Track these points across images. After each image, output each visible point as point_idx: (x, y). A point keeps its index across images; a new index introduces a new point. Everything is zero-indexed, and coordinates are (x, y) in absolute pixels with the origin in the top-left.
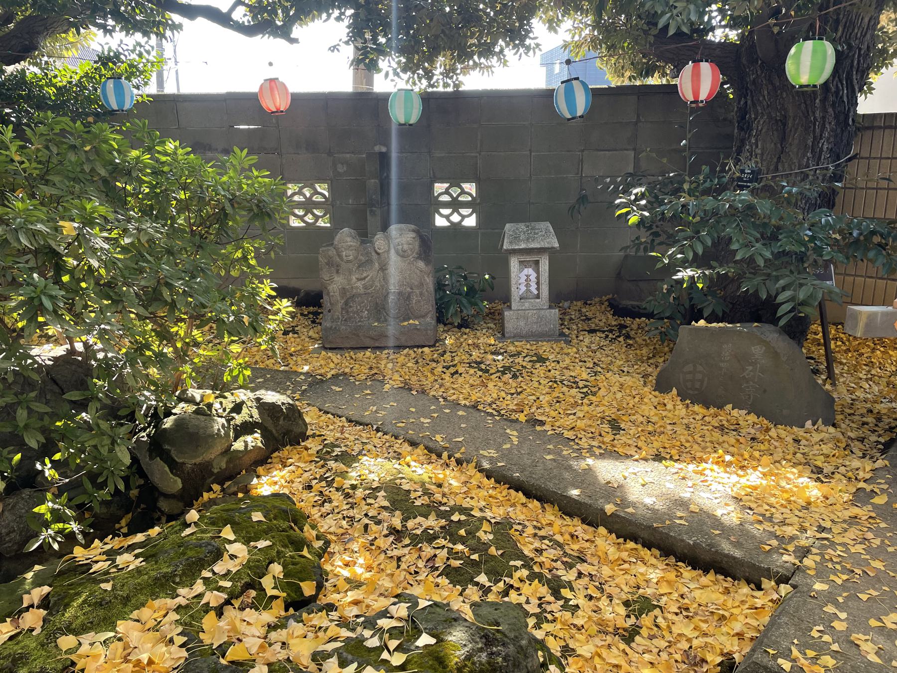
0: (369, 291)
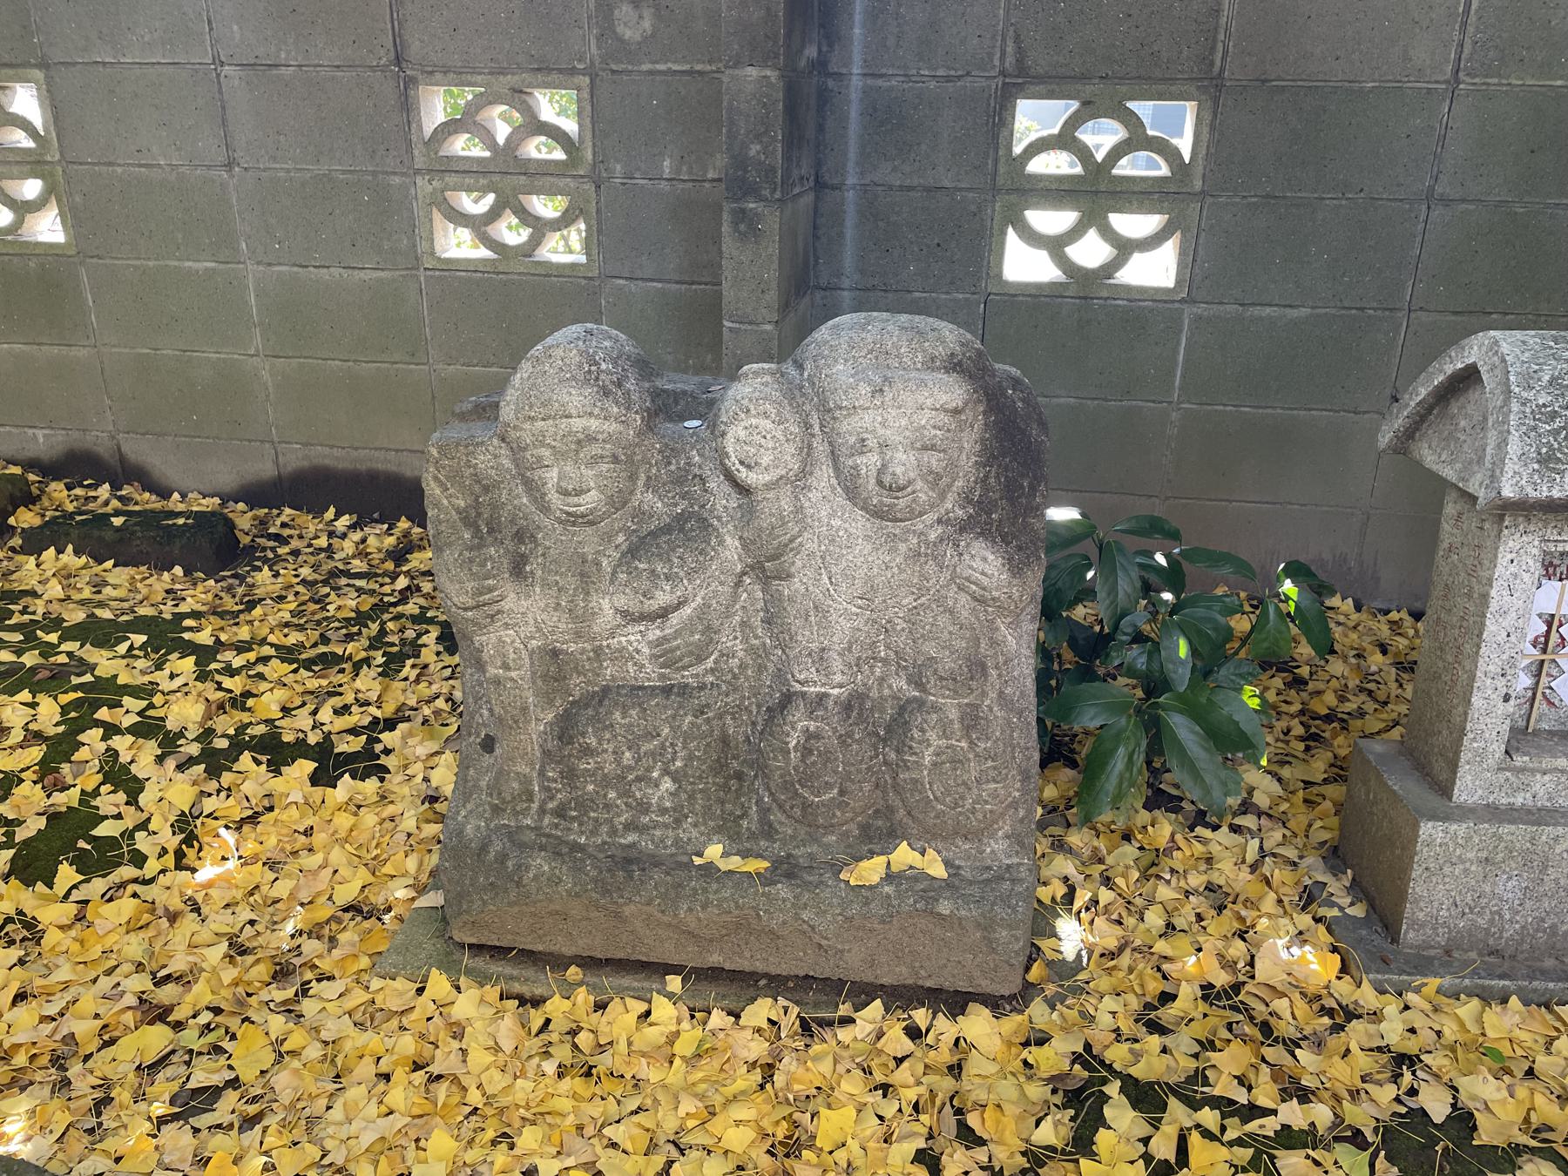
0: (688, 676)
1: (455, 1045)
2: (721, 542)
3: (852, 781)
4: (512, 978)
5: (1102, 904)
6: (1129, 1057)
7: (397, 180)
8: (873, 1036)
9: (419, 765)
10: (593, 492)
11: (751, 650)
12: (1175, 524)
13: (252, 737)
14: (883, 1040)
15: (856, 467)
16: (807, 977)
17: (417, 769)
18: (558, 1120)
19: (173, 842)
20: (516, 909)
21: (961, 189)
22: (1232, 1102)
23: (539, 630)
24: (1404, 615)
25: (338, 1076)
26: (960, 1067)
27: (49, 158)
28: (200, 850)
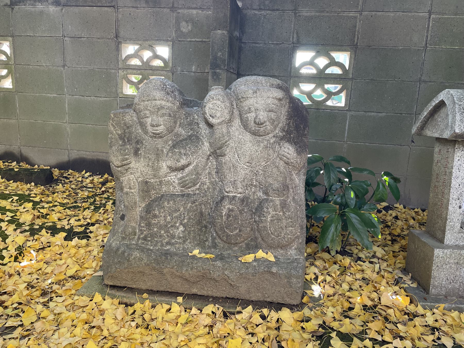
0: (190, 191)
1: (101, 317)
2: (203, 144)
3: (244, 227)
4: (124, 297)
5: (327, 281)
6: (339, 326)
7: (113, 71)
8: (249, 318)
9: (101, 236)
10: (162, 126)
11: (211, 183)
12: (348, 160)
13: (47, 226)
14: (252, 319)
15: (247, 118)
16: (227, 298)
17: (100, 238)
18: (135, 341)
19: (14, 253)
20: (127, 270)
21: (281, 76)
22: (376, 340)
23: (142, 174)
24: (419, 210)
25: (58, 325)
26: (279, 329)
27: (10, 63)
28: (24, 256)
